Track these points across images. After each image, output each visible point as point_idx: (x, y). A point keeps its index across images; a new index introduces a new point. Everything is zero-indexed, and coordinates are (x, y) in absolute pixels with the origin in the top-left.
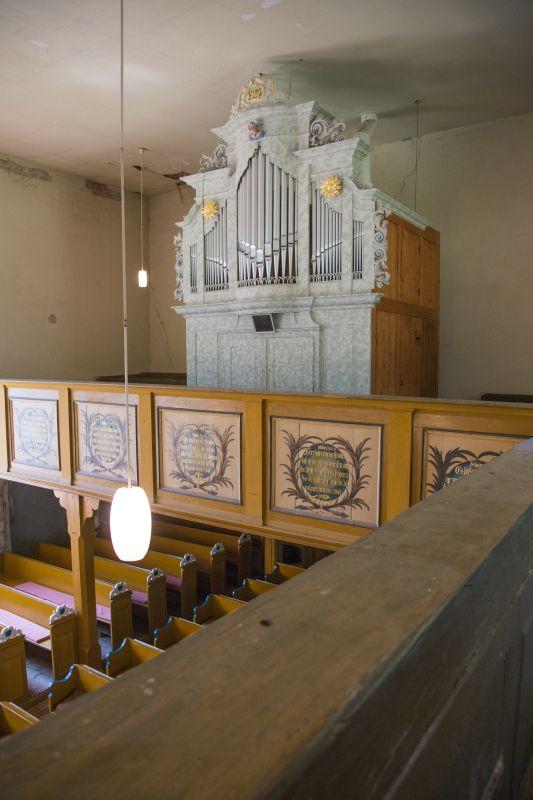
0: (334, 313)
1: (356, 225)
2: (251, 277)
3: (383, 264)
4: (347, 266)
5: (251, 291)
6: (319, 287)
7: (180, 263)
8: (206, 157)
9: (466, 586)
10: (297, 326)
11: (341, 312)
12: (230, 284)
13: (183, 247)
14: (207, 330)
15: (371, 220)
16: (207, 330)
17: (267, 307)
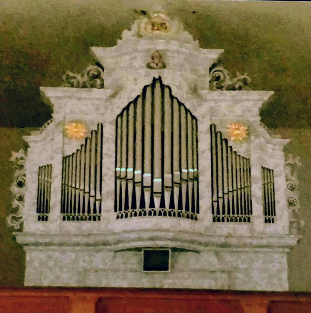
0: (243, 256)
1: (267, 172)
2: (89, 212)
3: (296, 211)
4: (258, 208)
5: (147, 222)
6: (225, 228)
7: (21, 184)
8: (71, 74)
9: (285, 126)
10: (198, 267)
11: (253, 256)
12: (103, 215)
13: (27, 166)
14: (61, 268)
15: (282, 168)
16: (61, 268)
17: (172, 240)
